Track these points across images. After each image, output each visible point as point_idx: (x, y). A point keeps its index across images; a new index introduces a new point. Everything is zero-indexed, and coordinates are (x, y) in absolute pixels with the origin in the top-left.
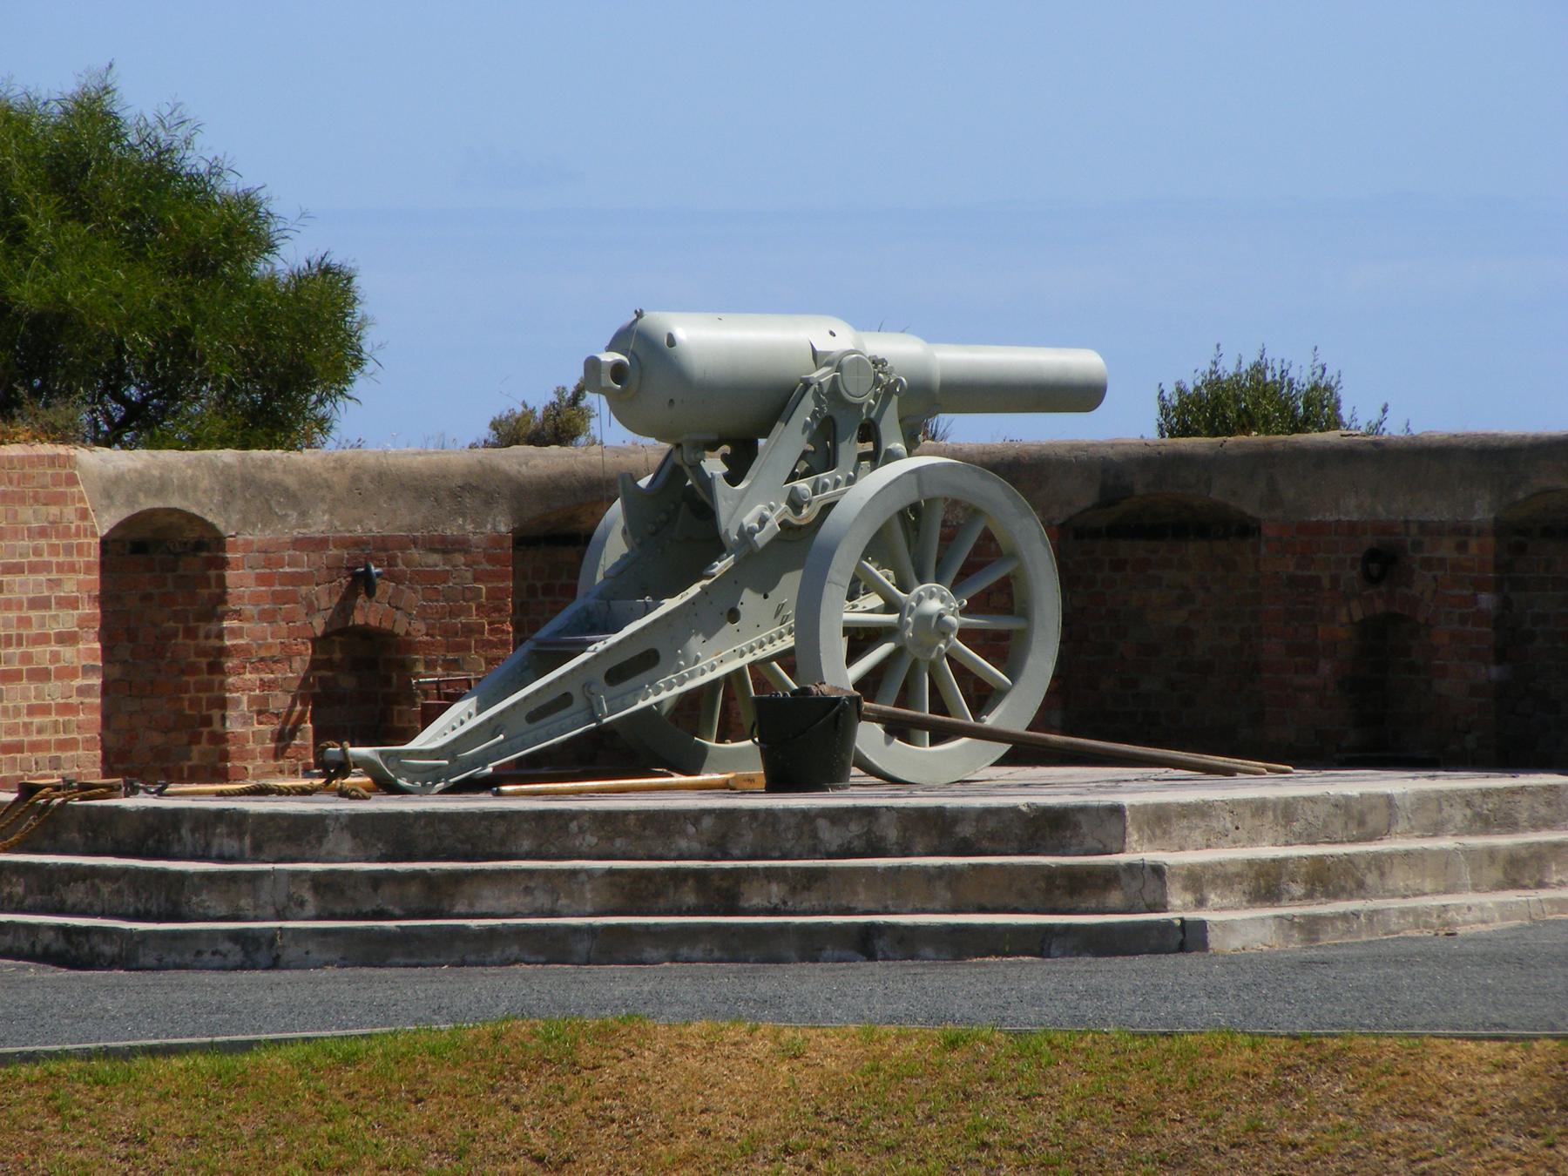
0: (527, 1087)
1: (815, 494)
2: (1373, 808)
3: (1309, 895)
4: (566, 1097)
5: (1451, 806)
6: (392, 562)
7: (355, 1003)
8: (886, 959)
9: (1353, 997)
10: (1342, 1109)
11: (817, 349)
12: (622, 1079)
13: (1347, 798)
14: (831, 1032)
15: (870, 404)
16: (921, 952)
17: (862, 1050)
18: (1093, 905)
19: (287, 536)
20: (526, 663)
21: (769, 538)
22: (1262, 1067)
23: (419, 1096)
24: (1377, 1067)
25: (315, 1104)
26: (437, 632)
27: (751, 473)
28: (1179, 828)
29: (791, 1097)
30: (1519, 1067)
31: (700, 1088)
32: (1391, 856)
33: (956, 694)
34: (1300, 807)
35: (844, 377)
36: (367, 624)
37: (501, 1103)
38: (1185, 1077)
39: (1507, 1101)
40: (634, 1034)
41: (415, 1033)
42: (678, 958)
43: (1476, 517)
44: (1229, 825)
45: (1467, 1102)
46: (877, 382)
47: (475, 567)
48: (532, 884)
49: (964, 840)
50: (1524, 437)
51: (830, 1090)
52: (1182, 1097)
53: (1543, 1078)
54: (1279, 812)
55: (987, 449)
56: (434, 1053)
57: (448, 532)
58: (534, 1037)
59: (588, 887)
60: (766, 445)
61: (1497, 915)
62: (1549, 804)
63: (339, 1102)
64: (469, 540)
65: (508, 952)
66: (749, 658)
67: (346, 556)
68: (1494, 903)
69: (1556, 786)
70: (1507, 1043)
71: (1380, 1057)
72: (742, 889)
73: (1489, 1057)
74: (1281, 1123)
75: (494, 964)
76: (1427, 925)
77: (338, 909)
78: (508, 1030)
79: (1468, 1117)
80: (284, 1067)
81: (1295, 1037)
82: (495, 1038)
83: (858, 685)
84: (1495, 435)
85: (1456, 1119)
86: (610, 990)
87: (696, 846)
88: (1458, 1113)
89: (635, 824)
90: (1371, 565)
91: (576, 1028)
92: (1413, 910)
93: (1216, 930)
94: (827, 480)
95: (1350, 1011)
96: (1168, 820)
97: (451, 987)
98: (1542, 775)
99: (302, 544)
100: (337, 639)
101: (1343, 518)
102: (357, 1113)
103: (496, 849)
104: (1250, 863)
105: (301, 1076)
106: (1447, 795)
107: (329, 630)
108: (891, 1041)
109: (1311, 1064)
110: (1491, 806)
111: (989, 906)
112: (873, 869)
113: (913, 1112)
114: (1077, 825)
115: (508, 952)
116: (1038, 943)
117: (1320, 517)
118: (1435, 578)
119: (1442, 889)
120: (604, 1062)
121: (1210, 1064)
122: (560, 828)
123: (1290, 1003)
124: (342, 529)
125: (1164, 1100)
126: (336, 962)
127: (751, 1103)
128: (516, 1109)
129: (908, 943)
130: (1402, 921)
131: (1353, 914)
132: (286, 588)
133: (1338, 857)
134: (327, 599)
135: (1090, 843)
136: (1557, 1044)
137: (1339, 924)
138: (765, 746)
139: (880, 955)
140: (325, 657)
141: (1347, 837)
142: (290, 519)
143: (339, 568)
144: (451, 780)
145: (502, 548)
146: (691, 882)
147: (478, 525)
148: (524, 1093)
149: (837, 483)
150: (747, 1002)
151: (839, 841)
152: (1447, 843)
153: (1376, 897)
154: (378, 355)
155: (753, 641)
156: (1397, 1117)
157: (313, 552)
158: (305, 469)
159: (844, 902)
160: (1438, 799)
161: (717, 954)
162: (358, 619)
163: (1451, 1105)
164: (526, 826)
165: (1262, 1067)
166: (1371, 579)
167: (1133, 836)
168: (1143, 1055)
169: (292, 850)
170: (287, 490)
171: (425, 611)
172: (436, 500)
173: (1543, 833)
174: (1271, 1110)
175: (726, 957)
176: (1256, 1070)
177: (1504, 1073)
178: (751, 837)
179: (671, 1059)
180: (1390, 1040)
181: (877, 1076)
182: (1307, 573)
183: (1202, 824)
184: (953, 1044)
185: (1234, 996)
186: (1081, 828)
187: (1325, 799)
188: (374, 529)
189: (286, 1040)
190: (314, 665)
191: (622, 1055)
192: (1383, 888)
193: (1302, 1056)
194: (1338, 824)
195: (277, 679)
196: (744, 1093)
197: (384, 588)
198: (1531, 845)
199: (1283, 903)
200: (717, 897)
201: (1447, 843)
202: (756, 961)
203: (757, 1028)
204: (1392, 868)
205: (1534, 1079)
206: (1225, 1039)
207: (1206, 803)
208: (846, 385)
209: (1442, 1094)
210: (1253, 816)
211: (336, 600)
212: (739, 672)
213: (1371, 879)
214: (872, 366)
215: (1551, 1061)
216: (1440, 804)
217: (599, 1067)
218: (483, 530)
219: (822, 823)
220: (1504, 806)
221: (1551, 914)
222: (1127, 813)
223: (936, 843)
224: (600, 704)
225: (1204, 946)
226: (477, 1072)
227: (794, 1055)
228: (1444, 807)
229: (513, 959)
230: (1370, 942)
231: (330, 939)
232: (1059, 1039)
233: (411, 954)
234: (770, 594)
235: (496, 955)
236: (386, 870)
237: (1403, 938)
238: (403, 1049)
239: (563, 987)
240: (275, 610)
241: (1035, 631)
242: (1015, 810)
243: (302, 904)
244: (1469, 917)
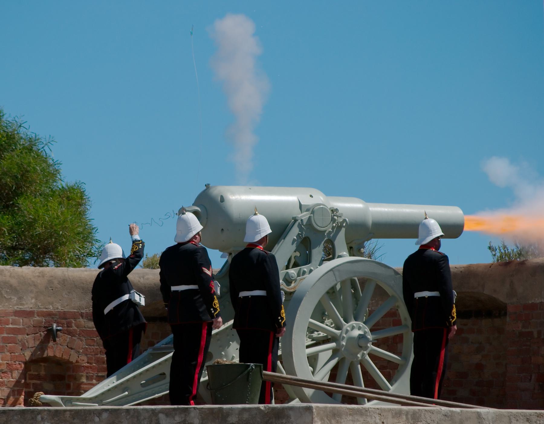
5: (517, 420)
6: (69, 325)
19: (11, 309)
26: (93, 361)
34: (423, 415)
36: (55, 356)
54: (409, 416)
67: (44, 321)
89: (69, 417)
99: (18, 313)
106: (515, 415)
114: (288, 417)
117: (533, 301)
124: (42, 307)
132: (10, 336)
134: (33, 342)
140: (36, 373)
142: (12, 300)
143: (40, 327)
157: (26, 318)
158: (22, 276)
160: (508, 416)
162: (49, 353)
170: (11, 286)
171: (87, 351)
182: (527, 330)
186: (291, 418)
188: (59, 307)
190: (24, 374)
210: (393, 417)
211: (38, 343)
216: (510, 419)
219: (161, 416)
222: (314, 410)
228: (513, 421)
240: (3, 346)
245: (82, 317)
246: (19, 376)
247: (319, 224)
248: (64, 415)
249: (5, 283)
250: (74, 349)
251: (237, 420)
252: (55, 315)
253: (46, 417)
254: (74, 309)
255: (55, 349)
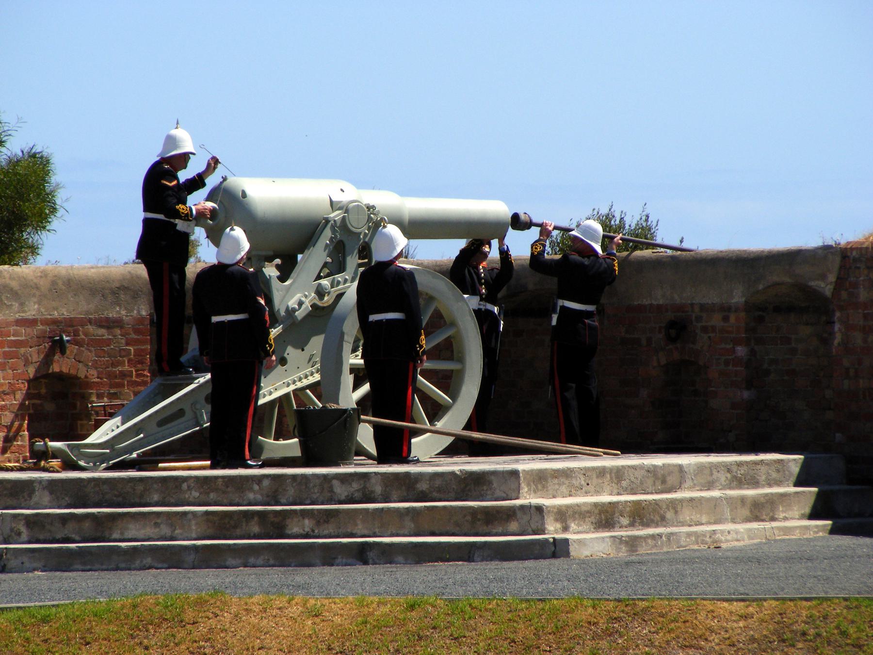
0: (153, 635)
1: (332, 287)
2: (671, 473)
3: (632, 525)
4: (176, 641)
6: (76, 333)
7: (50, 590)
8: (374, 563)
9: (656, 580)
10: (647, 643)
11: (334, 199)
12: (211, 630)
13: (655, 466)
14: (337, 601)
15: (365, 233)
16: (396, 559)
17: (357, 611)
18: (500, 531)
19: (12, 317)
20: (157, 391)
21: (304, 314)
22: (599, 618)
23: (87, 640)
24: (669, 617)
25: (24, 646)
26: (104, 376)
27: (293, 275)
28: (552, 484)
29: (313, 639)
30: (755, 617)
31: (258, 635)
32: (681, 501)
33: (421, 412)
34: (626, 472)
35: (350, 217)
36: (61, 371)
37: (137, 644)
38: (552, 625)
39: (748, 637)
40: (218, 603)
41: (85, 604)
42: (248, 565)
43: (734, 301)
44: (583, 482)
45: (724, 638)
46: (369, 219)
47: (127, 336)
48: (159, 521)
49: (422, 492)
50: (763, 252)
51: (337, 635)
52: (551, 637)
53: (769, 623)
54: (613, 475)
55: (438, 263)
56: (96, 616)
57: (111, 315)
58: (157, 605)
59: (193, 522)
60: (302, 258)
61: (746, 537)
62: (778, 471)
63: (38, 645)
64: (123, 320)
65: (145, 562)
66: (292, 387)
67: (48, 330)
68: (744, 529)
69: (782, 460)
70: (748, 602)
71: (671, 612)
72: (287, 523)
73: (737, 611)
74: (610, 652)
75: (135, 569)
76: (704, 542)
77: (41, 537)
78: (142, 602)
79: (723, 647)
80: (5, 624)
81: (619, 601)
82: (134, 606)
83: (359, 403)
84: (745, 251)
85: (717, 648)
86: (206, 581)
87: (259, 497)
88: (718, 644)
89: (222, 484)
90: (670, 330)
91: (183, 600)
92: (695, 533)
93: (575, 545)
94: (339, 279)
95: (654, 588)
96: (546, 479)
97: (109, 581)
98: (774, 454)
99: (22, 322)
100: (43, 381)
101: (654, 302)
102: (49, 651)
103: (137, 500)
104: (596, 505)
105: (15, 629)
106: (715, 465)
107: (38, 375)
108: (375, 605)
109: (629, 616)
110: (742, 472)
111: (437, 532)
112: (367, 510)
113: (388, 648)
114: (490, 483)
115: (145, 562)
116: (466, 553)
117: (640, 302)
118: (709, 337)
119: (712, 521)
120: (200, 620)
121: (568, 617)
122: (176, 487)
123: (617, 584)
125: (539, 639)
126: (40, 568)
127: (289, 643)
128: (147, 648)
129: (388, 554)
130: (688, 540)
131: (658, 535)
132: (11, 349)
133: (650, 502)
134: (37, 356)
135: (498, 493)
136: (778, 603)
137: (650, 541)
138: (302, 439)
139: (371, 561)
140: (37, 392)
141: (655, 490)
142: (14, 307)
143: (44, 337)
144: (110, 462)
145: (143, 325)
146: (256, 519)
147: (129, 310)
148: (151, 639)
149: (346, 281)
150: (288, 586)
151: (346, 494)
152: (716, 493)
153: (673, 526)
154: (65, 205)
155: (295, 377)
156: (681, 647)
157: (28, 327)
158: (23, 277)
159: (349, 530)
160: (710, 468)
161: (272, 562)
162: (56, 368)
163: (713, 640)
164: (155, 486)
165: (599, 618)
166: (671, 339)
167: (524, 489)
168: (527, 612)
169: (14, 502)
170: (12, 289)
171: (97, 363)
172: (103, 296)
173: (774, 488)
174: (604, 644)
175: (277, 564)
176: (595, 620)
177: (745, 620)
178: (293, 491)
179: (240, 618)
180: (677, 602)
181: (366, 626)
183: (567, 482)
184: (412, 607)
185: (584, 580)
186: (493, 484)
187: (641, 467)
188: (65, 313)
189: (6, 608)
190: (28, 396)
191: (211, 615)
192: (677, 520)
193: (623, 611)
194: (650, 482)
195: (6, 405)
196: (285, 637)
197: (72, 349)
198: (767, 495)
199: (615, 530)
200: (272, 528)
201: (716, 493)
202: (296, 566)
203: (293, 599)
204: (682, 508)
205: (764, 624)
206: (577, 602)
207: (569, 469)
208: (351, 222)
209: (708, 633)
210: (597, 477)
211: (42, 356)
212: (287, 395)
213: (669, 515)
214: (366, 210)
215: (774, 613)
216: (711, 471)
217: (197, 623)
218: (132, 314)
219: (335, 483)
220: (750, 471)
221: (779, 536)
222: (521, 475)
223: (405, 494)
224: (202, 415)
225: (567, 554)
226: (123, 626)
227: (315, 614)
228: (714, 472)
229: (147, 566)
230: (668, 552)
231: (37, 555)
232: (476, 603)
233: (84, 564)
234: (305, 348)
235: (137, 563)
236: (70, 513)
237: (689, 550)
238: (78, 613)
239: (177, 580)
240: (5, 363)
241: (467, 372)
242: (453, 473)
243: (19, 534)
244: (729, 537)
245: (90, 323)
246: (22, 397)
247: (353, 225)
248: (216, 483)
249: (5, 286)
250: (82, 362)
251: (428, 486)
252: (61, 322)
253: (193, 485)
254: (81, 315)
255: (61, 363)
